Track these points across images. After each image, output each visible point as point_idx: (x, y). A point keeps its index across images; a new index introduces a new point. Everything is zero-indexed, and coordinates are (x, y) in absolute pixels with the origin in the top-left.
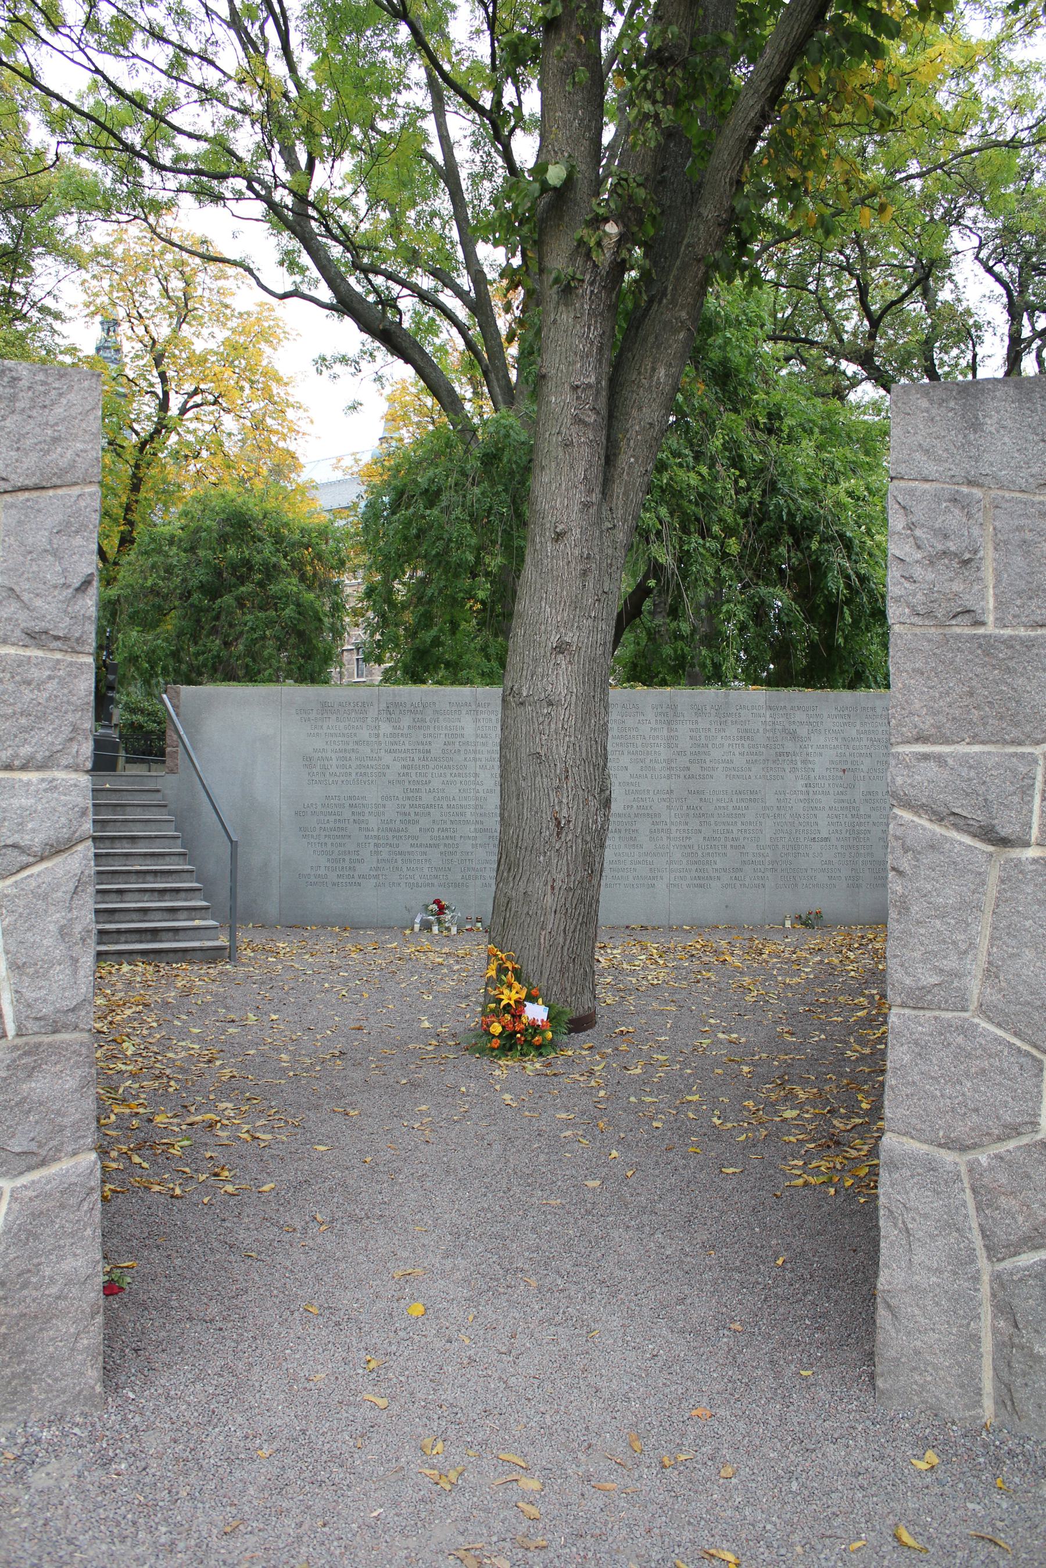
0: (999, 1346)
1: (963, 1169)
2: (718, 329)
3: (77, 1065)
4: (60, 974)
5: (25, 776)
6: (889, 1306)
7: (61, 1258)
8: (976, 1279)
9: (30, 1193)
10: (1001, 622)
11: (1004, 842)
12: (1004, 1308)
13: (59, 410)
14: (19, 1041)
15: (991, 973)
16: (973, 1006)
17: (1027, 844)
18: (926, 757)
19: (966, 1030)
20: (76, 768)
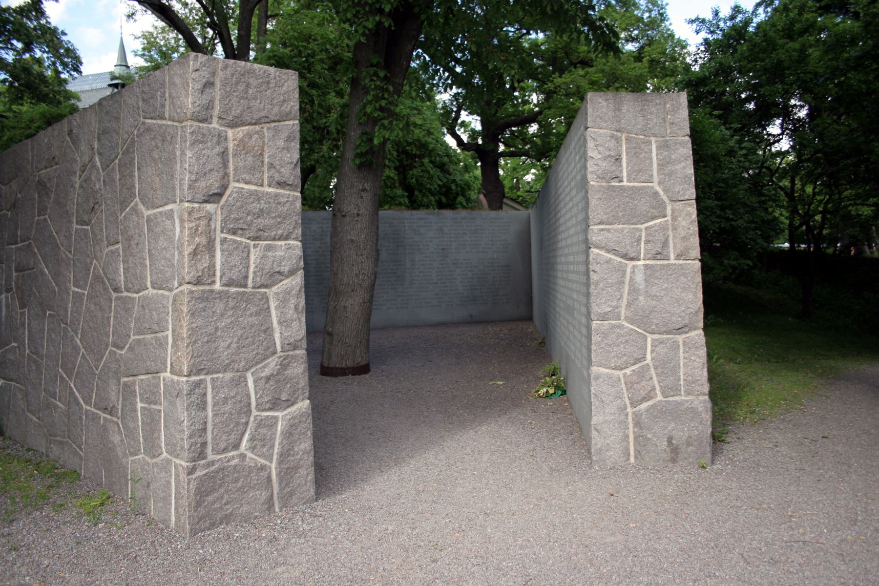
0: (635, 438)
1: (621, 376)
2: (721, 64)
3: (302, 363)
4: (295, 325)
5: (279, 243)
6: (596, 429)
7: (300, 444)
8: (627, 415)
9: (288, 417)
10: (628, 181)
11: (632, 259)
12: (637, 424)
13: (284, 88)
14: (282, 354)
15: (629, 305)
16: (622, 318)
17: (639, 260)
18: (603, 230)
19: (620, 327)
20: (296, 239)
